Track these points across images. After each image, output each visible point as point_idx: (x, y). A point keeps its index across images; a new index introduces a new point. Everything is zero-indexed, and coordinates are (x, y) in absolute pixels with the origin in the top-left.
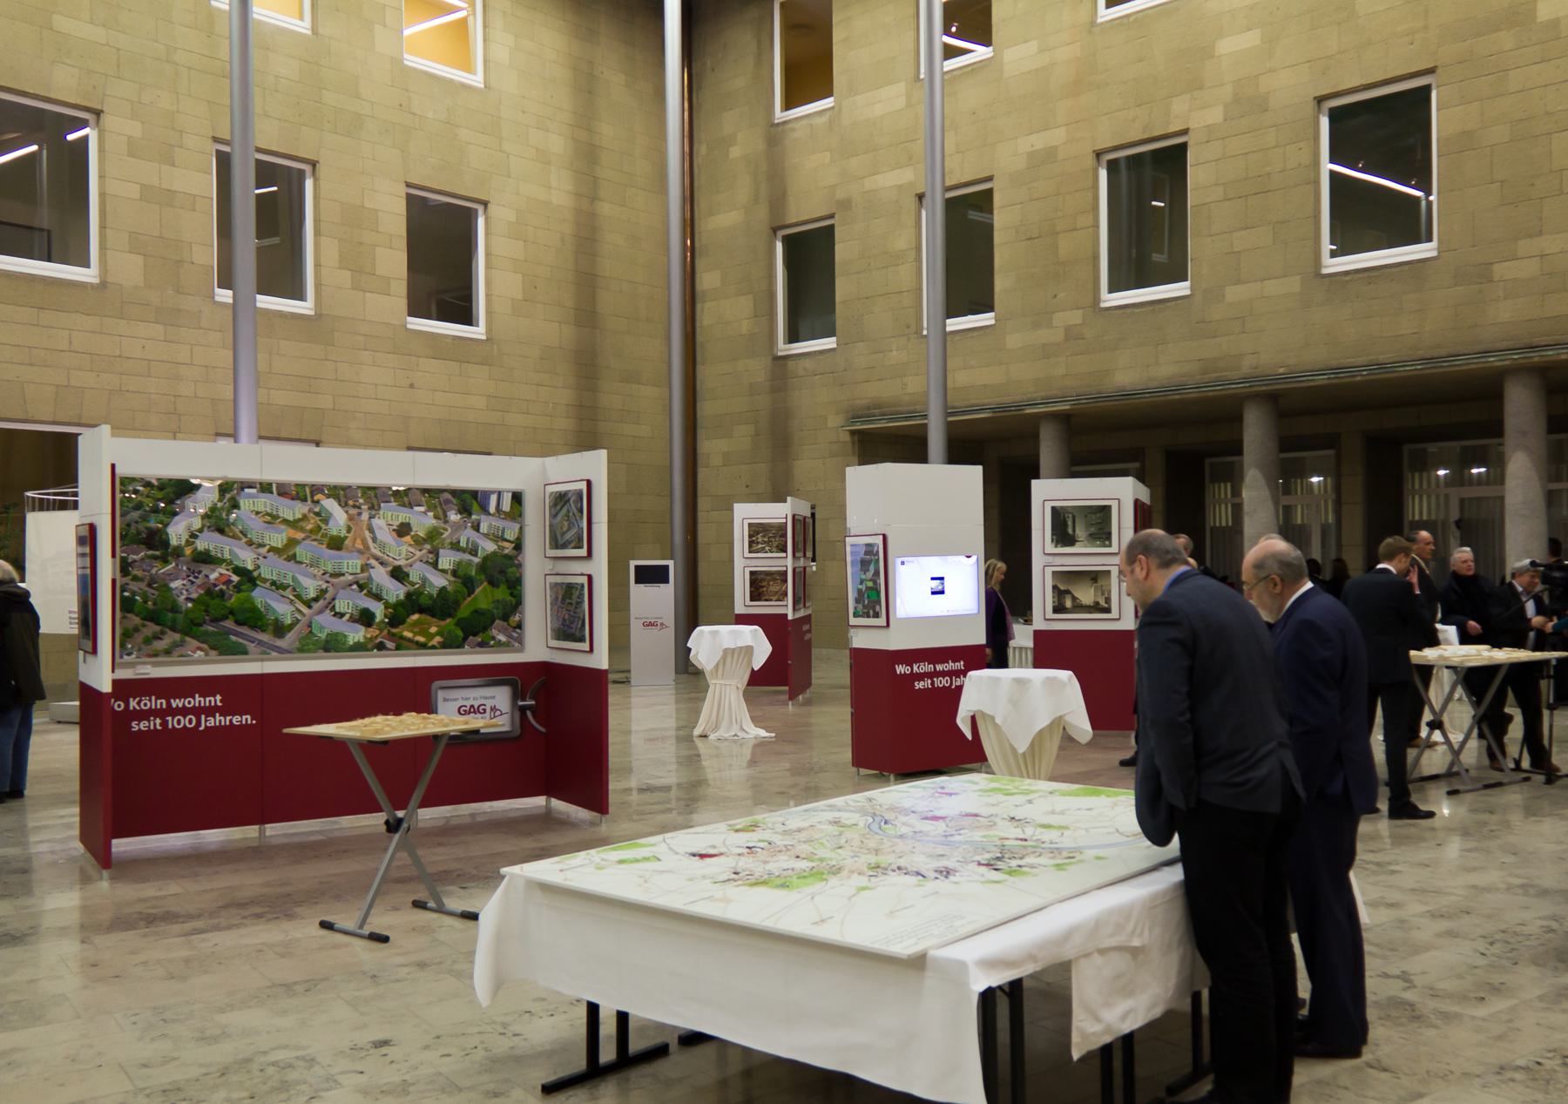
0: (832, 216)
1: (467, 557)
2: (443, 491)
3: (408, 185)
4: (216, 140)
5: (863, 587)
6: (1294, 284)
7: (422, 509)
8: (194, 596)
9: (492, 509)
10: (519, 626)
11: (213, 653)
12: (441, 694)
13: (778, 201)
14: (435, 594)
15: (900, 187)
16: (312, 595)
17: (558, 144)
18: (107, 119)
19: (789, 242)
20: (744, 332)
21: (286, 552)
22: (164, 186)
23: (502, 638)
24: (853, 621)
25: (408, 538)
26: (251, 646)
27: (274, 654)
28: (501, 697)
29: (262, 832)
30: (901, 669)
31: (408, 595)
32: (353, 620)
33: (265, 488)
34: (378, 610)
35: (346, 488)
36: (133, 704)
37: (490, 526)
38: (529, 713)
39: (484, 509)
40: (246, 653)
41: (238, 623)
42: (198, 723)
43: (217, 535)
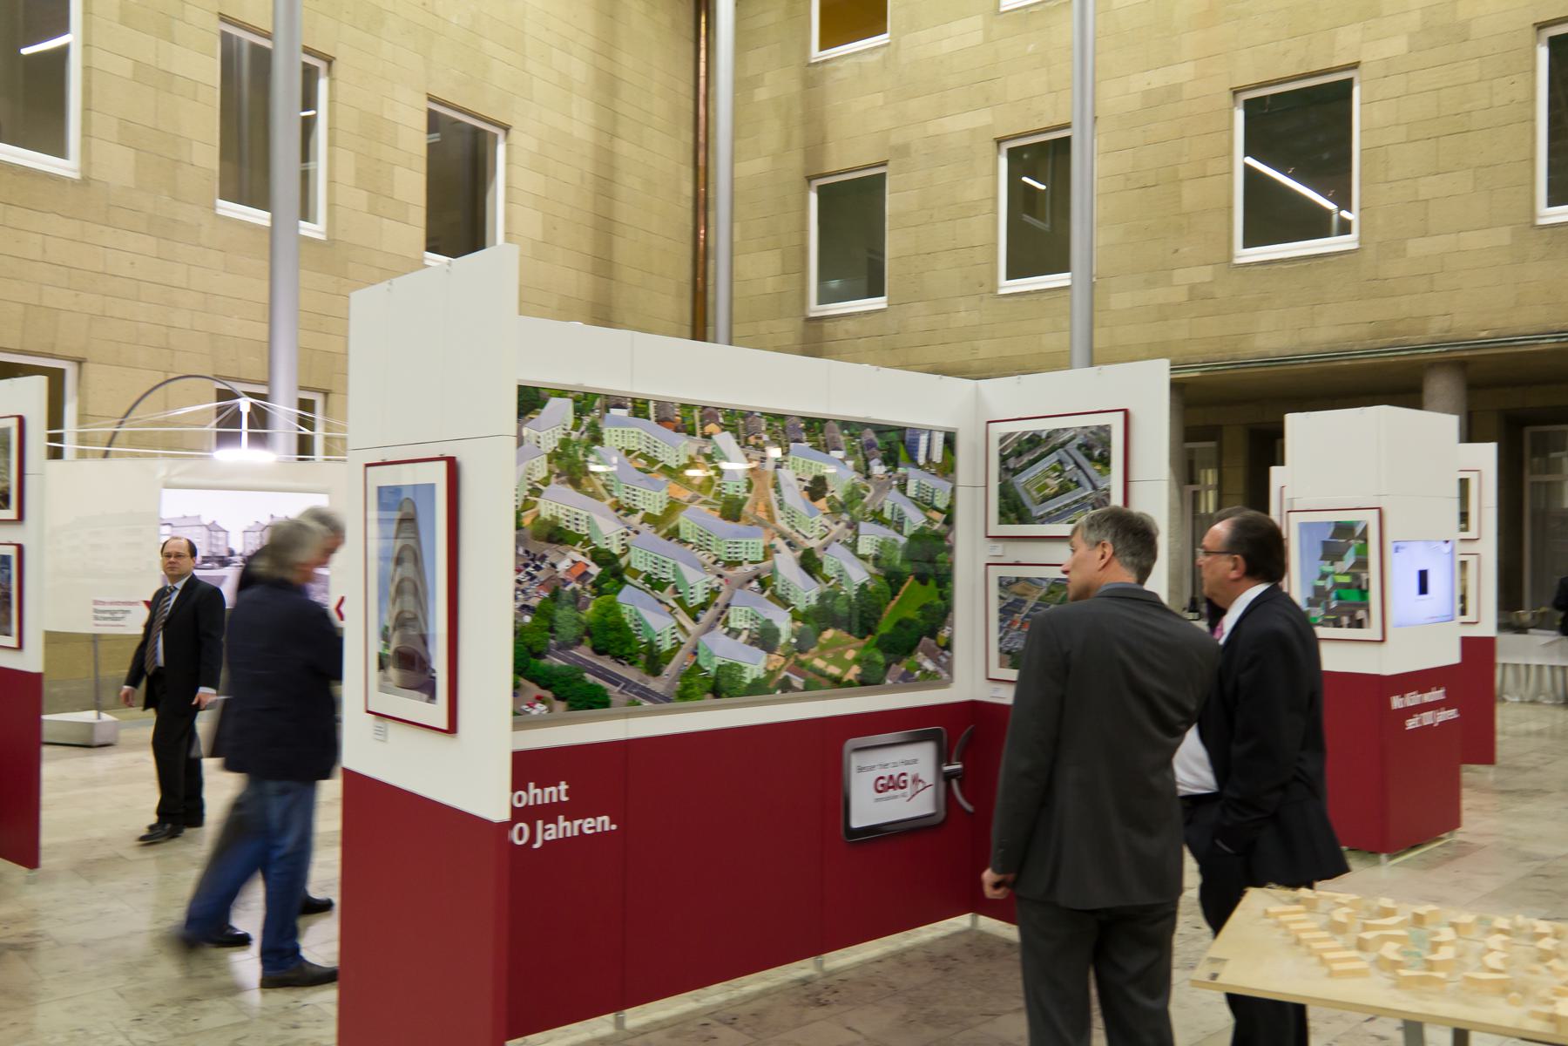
0: (884, 164)
1: (890, 534)
2: (865, 425)
3: (431, 99)
4: (223, 18)
5: (1328, 584)
6: (1503, 236)
7: (839, 454)
8: (534, 602)
9: (921, 460)
10: (948, 646)
11: (560, 706)
12: (856, 761)
13: (814, 148)
14: (853, 593)
15: (973, 131)
16: (700, 599)
17: (580, 70)
19: (822, 191)
20: (769, 290)
21: (665, 524)
22: (163, 66)
23: (929, 665)
24: (1321, 632)
25: (822, 503)
26: (613, 691)
27: (646, 704)
28: (920, 760)
29: (619, 1024)
31: (822, 597)
32: (753, 642)
33: (639, 408)
34: (784, 624)
35: (747, 415)
37: (919, 486)
38: (955, 783)
39: (913, 461)
40: (606, 704)
41: (598, 651)
42: (533, 838)
43: (569, 490)
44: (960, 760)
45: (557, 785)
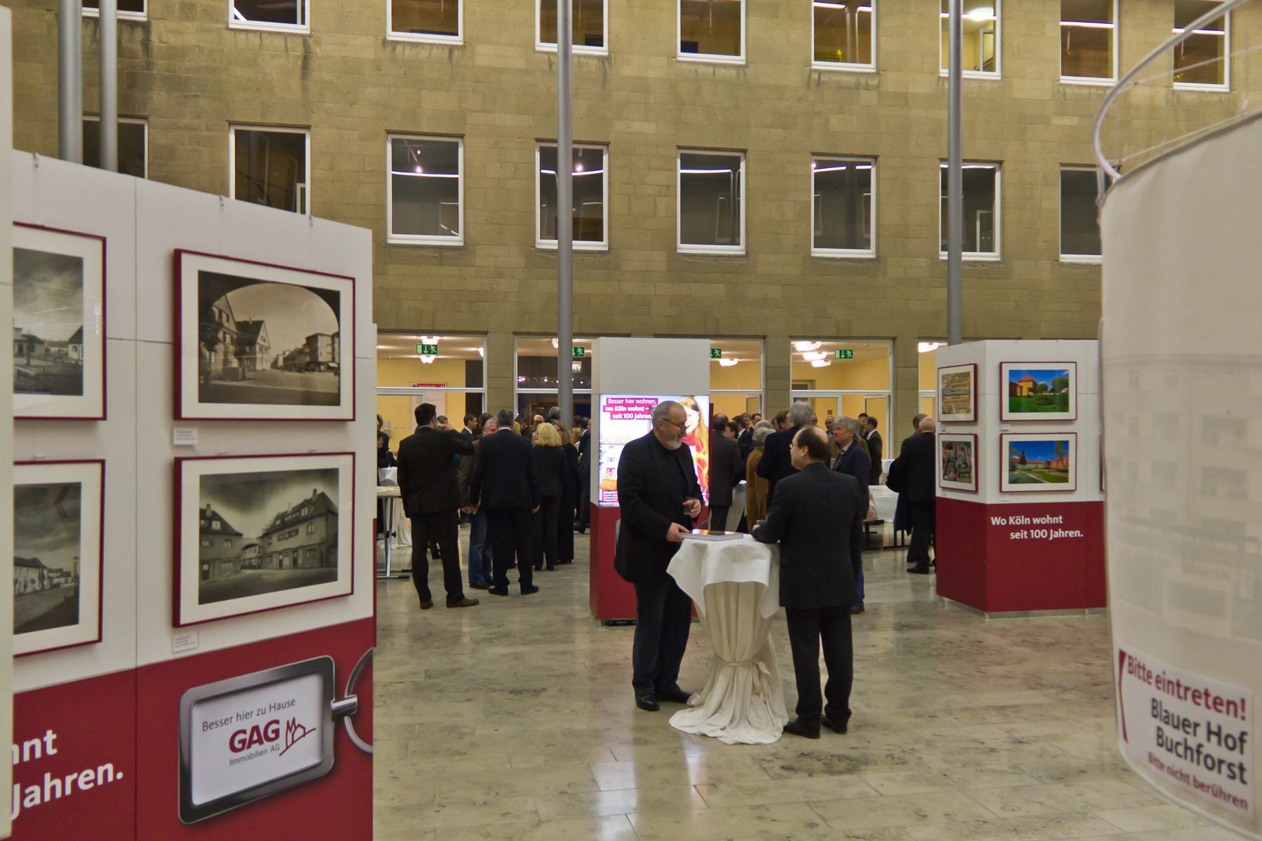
3: (679, 147)
12: (199, 716)
18: (881, 160)
28: (302, 699)
30: (996, 521)
36: (1011, 520)
38: (347, 721)
44: (355, 691)
45: (41, 736)
